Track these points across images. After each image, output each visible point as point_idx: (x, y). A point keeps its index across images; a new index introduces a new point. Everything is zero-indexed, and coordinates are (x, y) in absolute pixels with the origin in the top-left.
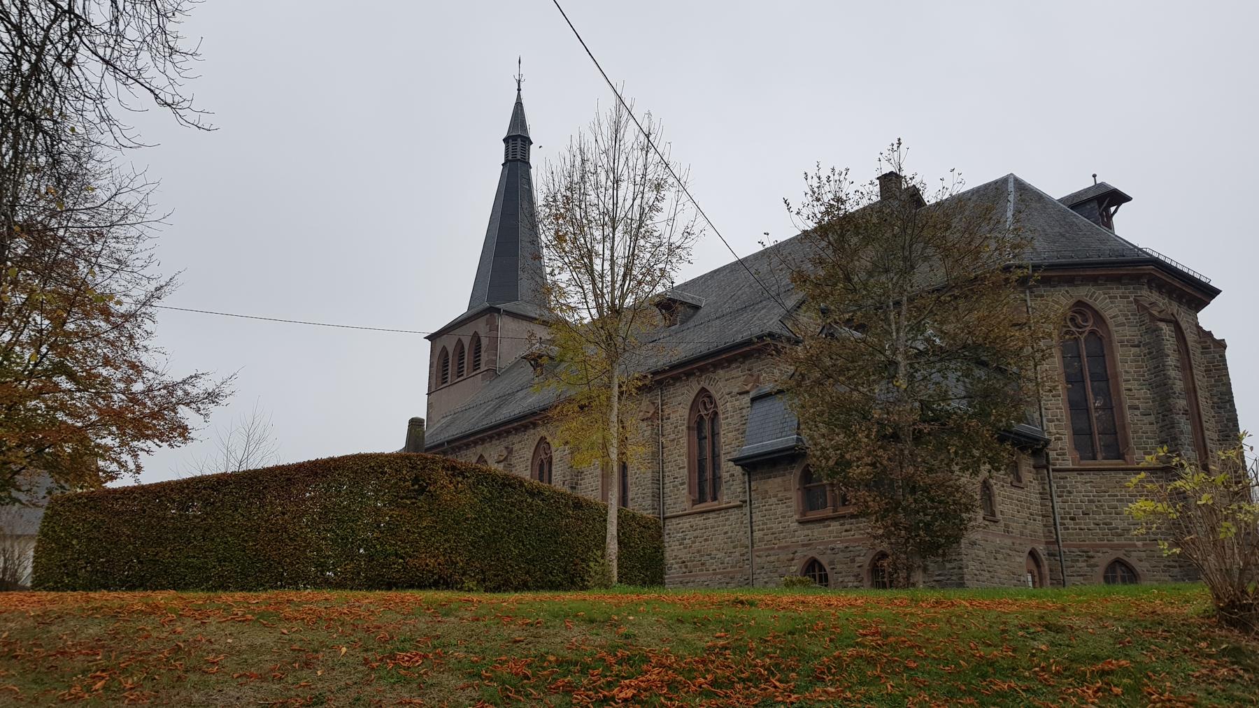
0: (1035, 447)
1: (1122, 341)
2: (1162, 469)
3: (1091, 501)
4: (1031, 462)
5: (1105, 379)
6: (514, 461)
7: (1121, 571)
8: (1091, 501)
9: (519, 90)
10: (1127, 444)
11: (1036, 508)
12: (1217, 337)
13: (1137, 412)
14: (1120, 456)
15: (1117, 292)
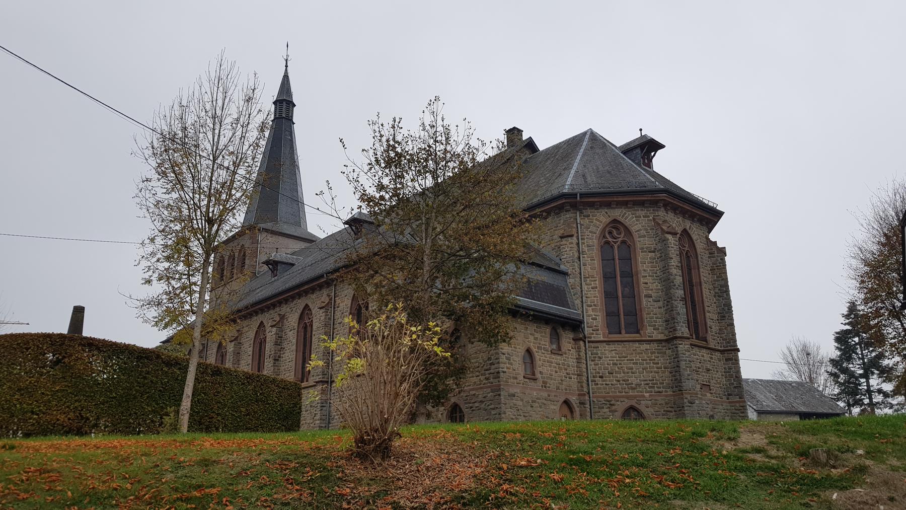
0: (575, 326)
1: (643, 248)
2: (666, 341)
3: (615, 364)
4: (571, 335)
5: (630, 276)
6: (243, 341)
7: (633, 412)
8: (615, 364)
9: (286, 66)
10: (642, 321)
11: (572, 370)
12: (720, 245)
13: (650, 300)
14: (638, 332)
15: (641, 213)
